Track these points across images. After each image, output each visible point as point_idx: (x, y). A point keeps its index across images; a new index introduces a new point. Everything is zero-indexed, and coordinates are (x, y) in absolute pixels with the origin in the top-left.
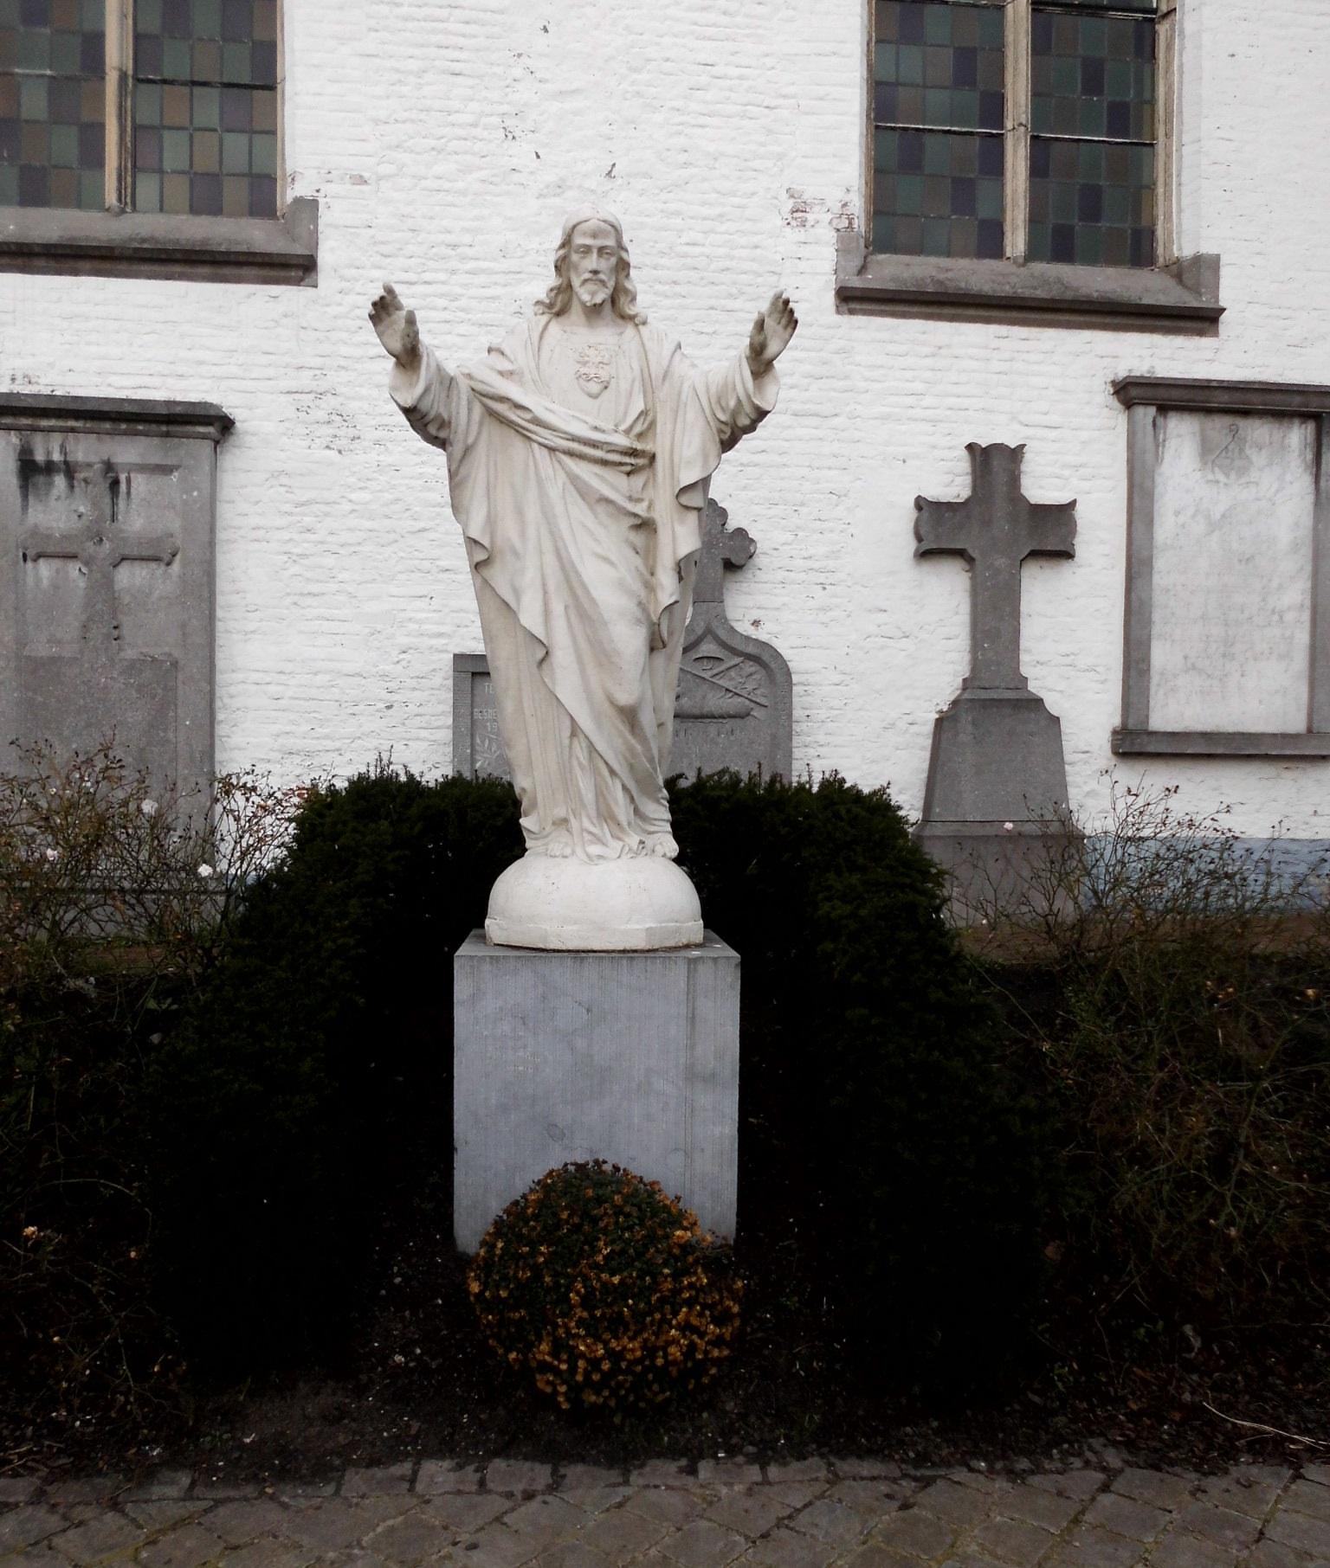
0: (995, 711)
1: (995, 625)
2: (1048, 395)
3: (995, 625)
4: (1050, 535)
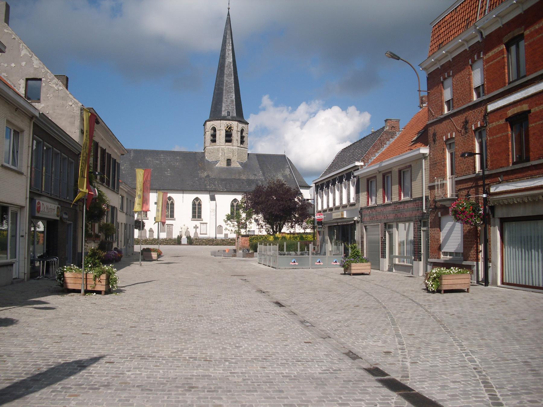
0: (196, 233)
1: (196, 230)
2: (197, 223)
3: (196, 230)
4: (198, 228)
